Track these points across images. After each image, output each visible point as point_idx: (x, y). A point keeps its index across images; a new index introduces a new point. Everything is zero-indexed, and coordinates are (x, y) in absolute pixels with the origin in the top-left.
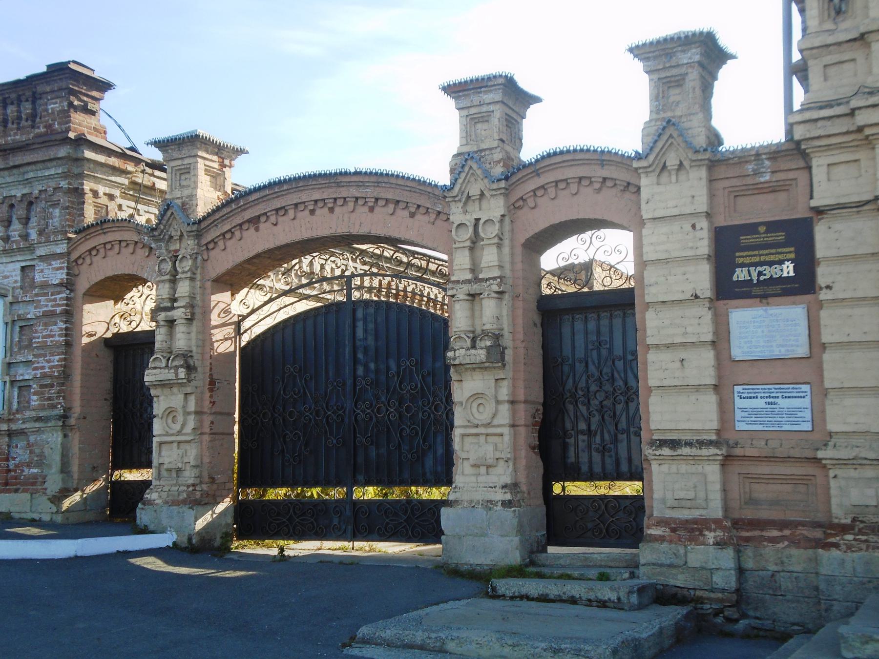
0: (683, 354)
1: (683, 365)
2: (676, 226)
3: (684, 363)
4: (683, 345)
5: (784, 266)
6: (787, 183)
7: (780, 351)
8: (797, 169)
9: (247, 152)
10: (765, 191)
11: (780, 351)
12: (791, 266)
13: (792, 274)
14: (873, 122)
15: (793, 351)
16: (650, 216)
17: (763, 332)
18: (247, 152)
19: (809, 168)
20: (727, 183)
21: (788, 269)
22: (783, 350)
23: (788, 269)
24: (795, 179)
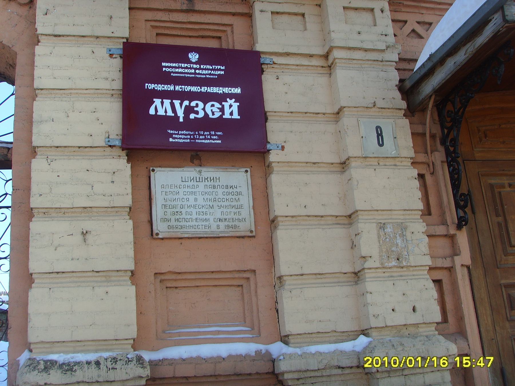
0: (87, 225)
1: (85, 240)
2: (85, 50)
3: (88, 236)
4: (86, 210)
5: (226, 105)
6: (221, 28)
7: (218, 226)
8: (42, 89)
9: (416, 22)
10: (191, 34)
11: (218, 226)
12: (236, 106)
13: (236, 116)
14: (216, 22)
15: (235, 226)
16: (49, 31)
17: (196, 200)
18: (416, 22)
19: (249, 16)
20: (149, 15)
21: (232, 110)
22: (222, 225)
23: (232, 110)
24: (231, 25)
